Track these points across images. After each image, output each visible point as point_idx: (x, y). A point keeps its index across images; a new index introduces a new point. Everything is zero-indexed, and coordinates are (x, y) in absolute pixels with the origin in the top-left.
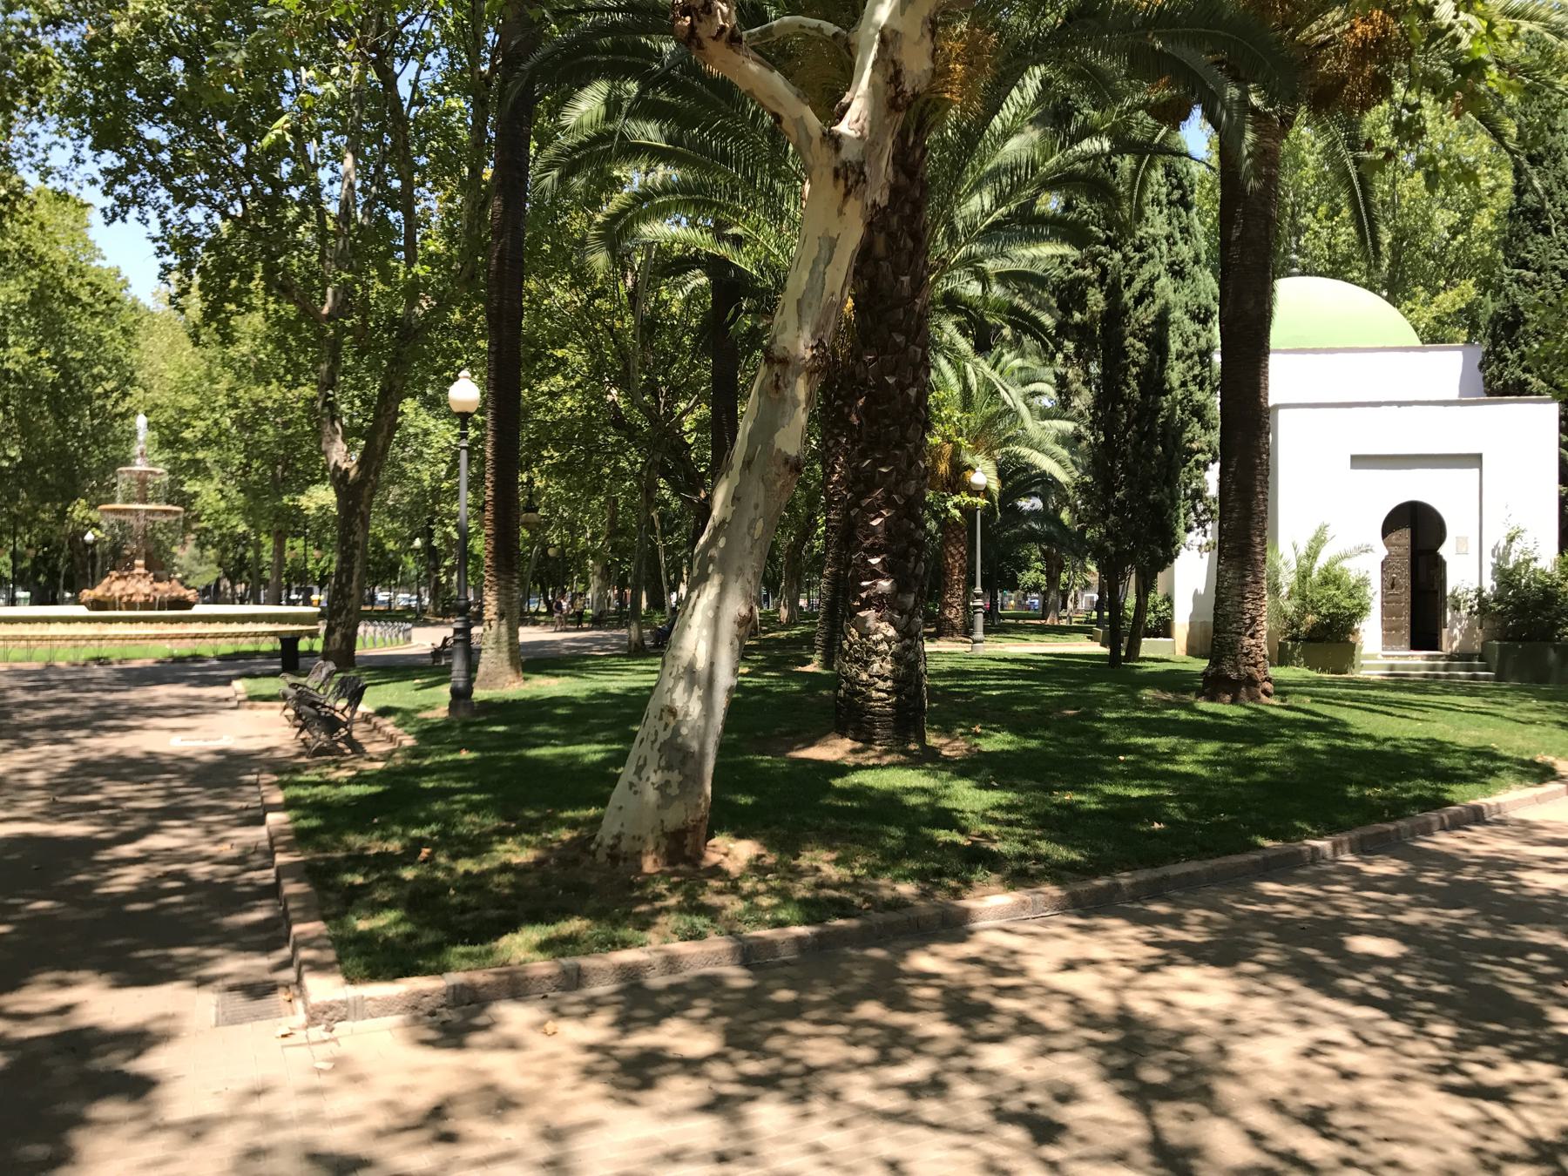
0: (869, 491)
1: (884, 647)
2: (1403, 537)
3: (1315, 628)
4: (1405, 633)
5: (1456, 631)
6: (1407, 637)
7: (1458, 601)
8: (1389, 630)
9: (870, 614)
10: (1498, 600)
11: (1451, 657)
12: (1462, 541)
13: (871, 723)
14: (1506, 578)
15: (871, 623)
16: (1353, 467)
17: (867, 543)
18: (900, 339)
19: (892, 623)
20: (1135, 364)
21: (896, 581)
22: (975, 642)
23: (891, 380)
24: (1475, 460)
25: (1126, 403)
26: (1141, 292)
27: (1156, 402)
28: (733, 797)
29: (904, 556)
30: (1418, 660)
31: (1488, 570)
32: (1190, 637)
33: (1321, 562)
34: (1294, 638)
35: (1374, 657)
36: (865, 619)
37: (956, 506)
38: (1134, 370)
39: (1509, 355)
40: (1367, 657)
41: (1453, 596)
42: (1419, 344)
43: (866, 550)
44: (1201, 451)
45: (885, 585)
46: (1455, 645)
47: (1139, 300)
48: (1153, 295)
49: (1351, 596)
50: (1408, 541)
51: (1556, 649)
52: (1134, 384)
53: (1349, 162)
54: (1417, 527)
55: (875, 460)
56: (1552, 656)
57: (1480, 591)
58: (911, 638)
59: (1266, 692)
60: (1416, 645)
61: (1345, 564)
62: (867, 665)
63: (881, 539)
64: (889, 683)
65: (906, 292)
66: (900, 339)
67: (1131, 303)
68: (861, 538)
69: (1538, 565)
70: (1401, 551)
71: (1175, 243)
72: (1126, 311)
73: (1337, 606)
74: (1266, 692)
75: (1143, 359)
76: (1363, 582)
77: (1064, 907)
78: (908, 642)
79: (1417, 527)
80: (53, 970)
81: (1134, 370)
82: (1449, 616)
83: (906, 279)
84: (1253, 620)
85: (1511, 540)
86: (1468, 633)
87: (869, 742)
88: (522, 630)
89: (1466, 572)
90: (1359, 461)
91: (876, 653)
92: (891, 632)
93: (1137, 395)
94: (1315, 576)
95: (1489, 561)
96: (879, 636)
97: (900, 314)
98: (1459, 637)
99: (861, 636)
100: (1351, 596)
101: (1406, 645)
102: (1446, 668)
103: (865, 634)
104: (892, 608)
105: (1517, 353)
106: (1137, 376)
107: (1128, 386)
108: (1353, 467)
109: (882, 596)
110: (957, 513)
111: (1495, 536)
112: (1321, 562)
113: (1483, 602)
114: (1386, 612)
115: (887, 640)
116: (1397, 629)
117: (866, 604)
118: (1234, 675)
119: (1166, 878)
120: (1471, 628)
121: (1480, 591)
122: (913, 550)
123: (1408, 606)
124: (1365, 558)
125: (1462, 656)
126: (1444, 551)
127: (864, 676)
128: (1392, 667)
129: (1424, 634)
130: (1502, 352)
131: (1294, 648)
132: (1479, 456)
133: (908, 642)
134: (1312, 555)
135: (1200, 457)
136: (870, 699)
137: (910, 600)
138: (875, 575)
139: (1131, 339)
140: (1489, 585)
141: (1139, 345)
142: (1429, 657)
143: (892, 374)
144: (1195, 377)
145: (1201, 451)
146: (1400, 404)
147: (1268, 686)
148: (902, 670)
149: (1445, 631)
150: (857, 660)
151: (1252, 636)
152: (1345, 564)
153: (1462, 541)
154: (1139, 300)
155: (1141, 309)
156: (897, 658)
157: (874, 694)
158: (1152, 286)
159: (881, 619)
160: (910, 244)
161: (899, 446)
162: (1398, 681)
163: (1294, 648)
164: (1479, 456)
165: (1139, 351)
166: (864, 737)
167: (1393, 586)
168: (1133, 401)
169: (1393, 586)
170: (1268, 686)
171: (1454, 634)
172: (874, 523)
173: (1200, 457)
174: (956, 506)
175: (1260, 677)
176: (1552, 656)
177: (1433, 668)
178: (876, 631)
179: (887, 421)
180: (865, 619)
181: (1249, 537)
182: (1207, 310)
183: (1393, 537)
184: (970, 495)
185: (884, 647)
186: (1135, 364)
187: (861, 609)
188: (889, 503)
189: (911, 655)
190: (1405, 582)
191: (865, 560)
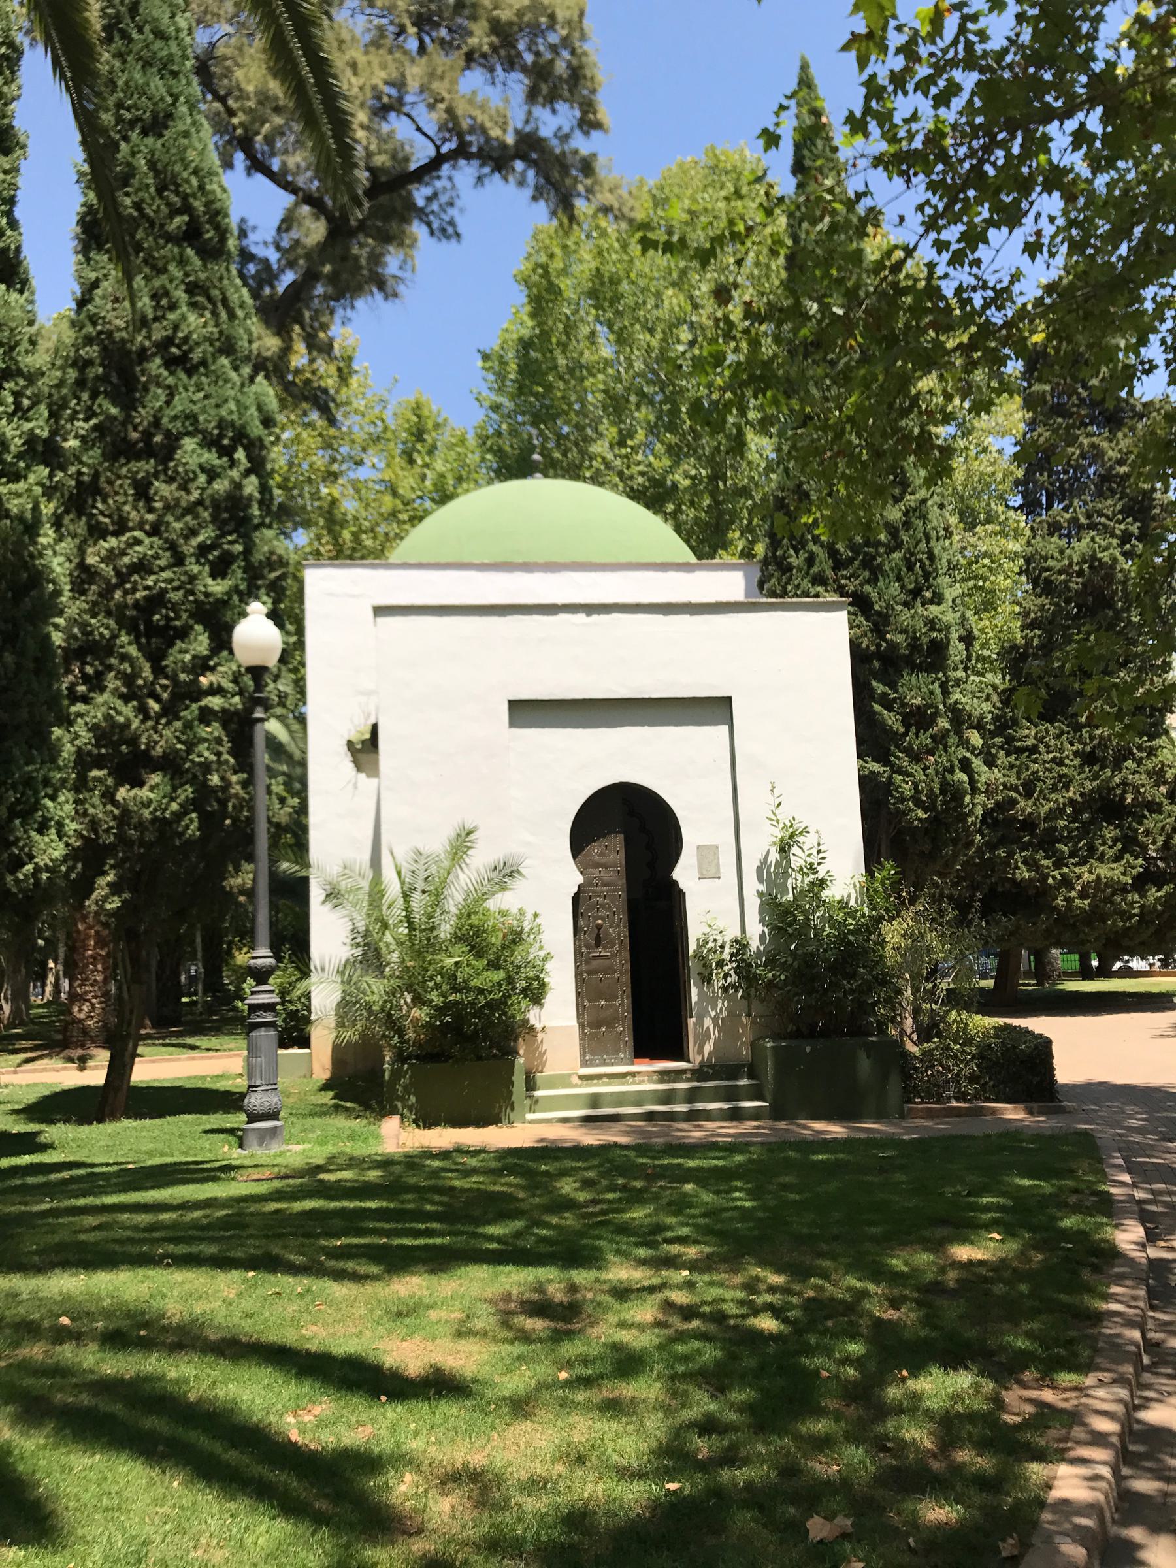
2: (611, 850)
4: (624, 1030)
5: (708, 1023)
6: (628, 1038)
7: (706, 965)
10: (771, 963)
11: (699, 1074)
12: (708, 853)
14: (782, 917)
16: (513, 723)
24: (716, 709)
31: (753, 905)
32: (340, 1054)
33: (454, 901)
35: (562, 1081)
39: (794, 561)
41: (698, 955)
42: (693, 559)
46: (708, 1047)
51: (869, 1048)
54: (629, 830)
56: (864, 1065)
57: (741, 945)
60: (644, 1048)
69: (833, 893)
70: (607, 876)
71: (173, 307)
73: (464, 988)
79: (629, 830)
80: (9, 1214)
82: (694, 991)
86: (727, 1026)
89: (718, 909)
90: (525, 712)
94: (445, 930)
95: (753, 886)
98: (714, 1035)
101: (626, 1052)
102: (692, 1096)
105: (803, 555)
108: (513, 723)
111: (760, 844)
112: (454, 901)
113: (745, 970)
116: (610, 1023)
120: (732, 1015)
121: (741, 945)
123: (627, 978)
124: (545, 897)
126: (678, 874)
129: (655, 1025)
130: (784, 557)
132: (728, 701)
140: (755, 930)
142: (664, 1075)
144: (203, 550)
149: (691, 1021)
164: (728, 701)
167: (598, 942)
169: (598, 942)
171: (708, 1020)
176: (864, 1065)
177: (667, 1097)
190: (618, 931)
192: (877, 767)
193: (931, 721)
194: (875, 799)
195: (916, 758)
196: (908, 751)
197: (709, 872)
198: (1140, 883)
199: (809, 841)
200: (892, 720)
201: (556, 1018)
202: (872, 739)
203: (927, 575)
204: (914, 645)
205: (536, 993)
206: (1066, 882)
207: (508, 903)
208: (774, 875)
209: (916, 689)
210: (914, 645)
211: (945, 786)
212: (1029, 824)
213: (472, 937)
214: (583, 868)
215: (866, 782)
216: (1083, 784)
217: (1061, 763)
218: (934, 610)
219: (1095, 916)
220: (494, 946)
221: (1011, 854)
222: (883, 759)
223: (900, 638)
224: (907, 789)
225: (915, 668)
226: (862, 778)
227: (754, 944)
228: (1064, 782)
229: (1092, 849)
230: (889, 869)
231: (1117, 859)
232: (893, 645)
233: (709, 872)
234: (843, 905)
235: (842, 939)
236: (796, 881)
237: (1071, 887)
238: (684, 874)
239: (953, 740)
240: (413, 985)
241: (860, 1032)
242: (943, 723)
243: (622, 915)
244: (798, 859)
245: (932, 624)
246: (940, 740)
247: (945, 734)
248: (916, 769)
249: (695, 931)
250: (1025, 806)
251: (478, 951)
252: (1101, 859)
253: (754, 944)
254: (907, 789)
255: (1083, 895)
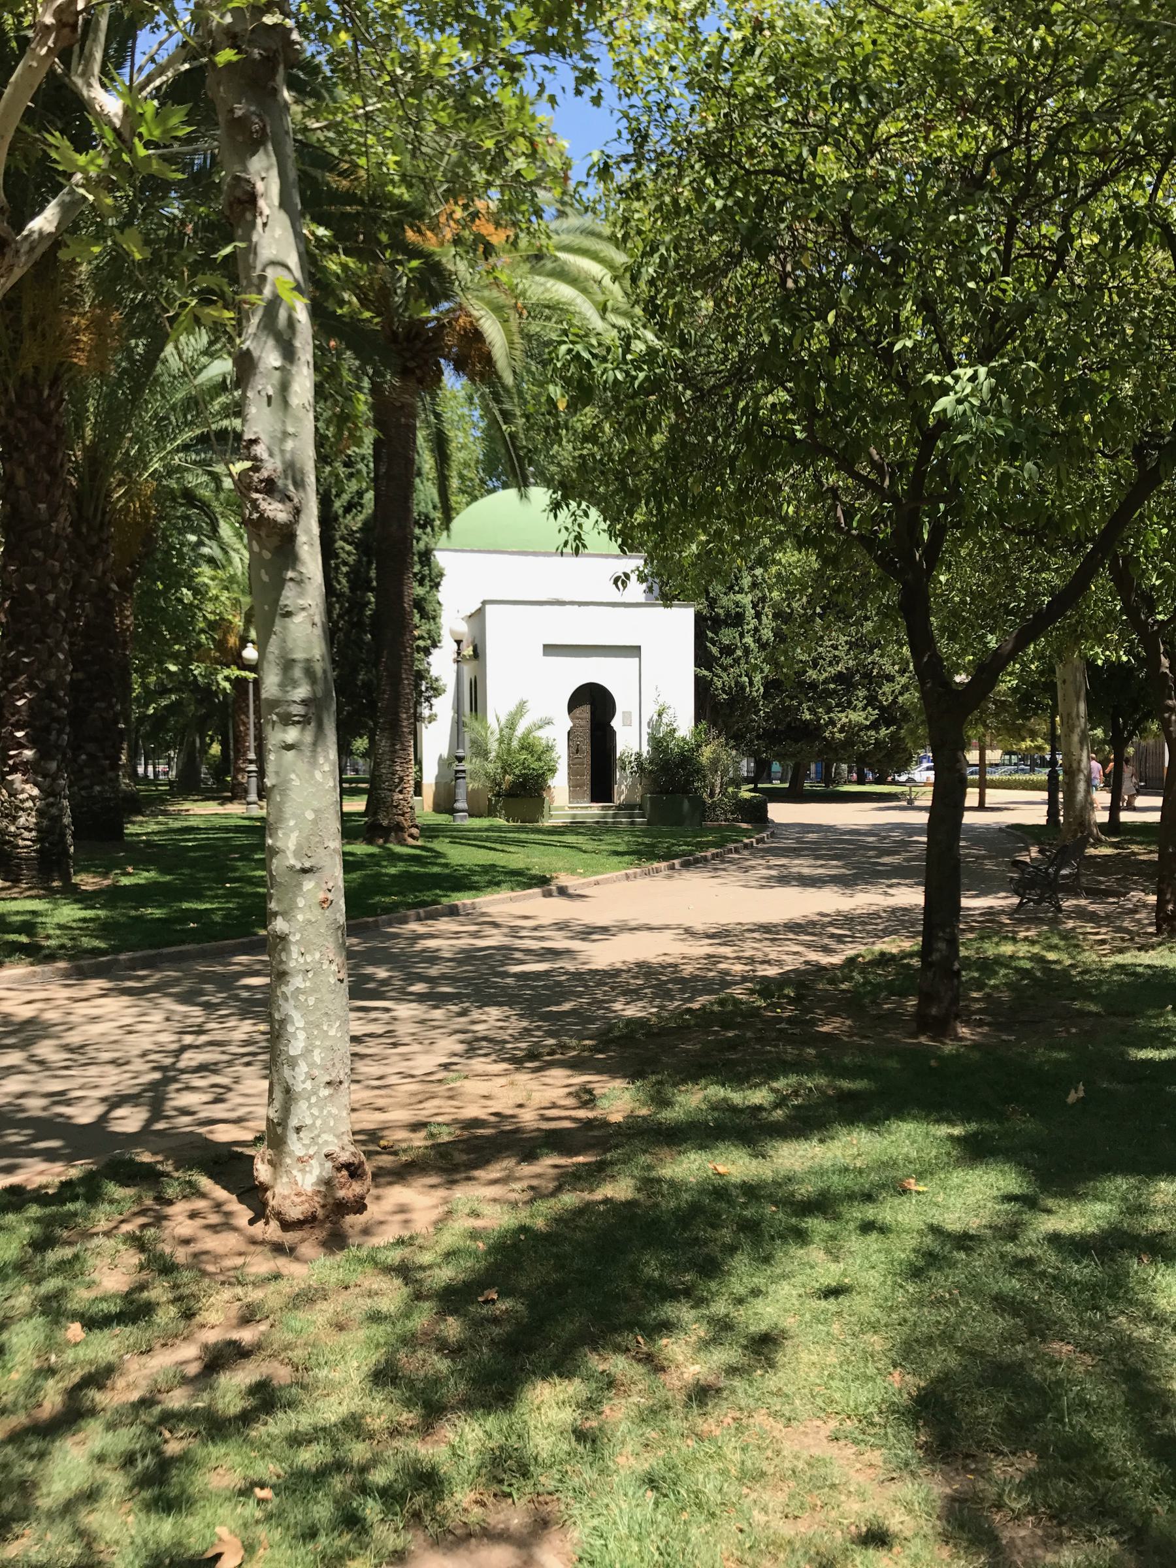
0: (13, 678)
1: (29, 804)
2: (585, 711)
3: (514, 785)
4: (587, 789)
8: (574, 786)
9: (17, 777)
11: (619, 808)
12: (627, 715)
13: (18, 866)
14: (657, 744)
15: (18, 785)
17: (13, 720)
18: (39, 554)
19: (36, 784)
20: (345, 564)
21: (38, 751)
22: (249, 803)
23: (31, 587)
24: (634, 651)
25: (338, 596)
26: (349, 502)
27: (363, 597)
28: (973, 1127)
29: (47, 730)
30: (593, 811)
31: (645, 738)
32: (437, 795)
33: (520, 731)
34: (498, 795)
35: (562, 808)
36: (12, 782)
37: (227, 678)
38: (345, 569)
40: (557, 809)
43: (12, 725)
44: (421, 638)
45: (28, 753)
47: (348, 509)
48: (362, 506)
49: (539, 759)
50: (588, 716)
51: (690, 799)
52: (344, 581)
53: (497, 413)
54: (594, 703)
55: (18, 652)
56: (686, 805)
57: (639, 755)
58: (55, 796)
59: (411, 836)
60: (595, 799)
61: (539, 734)
62: (15, 819)
63: (24, 716)
64: (34, 833)
65: (44, 516)
66: (39, 554)
67: (340, 512)
68: (7, 715)
70: (583, 723)
72: (336, 518)
73: (528, 768)
74: (411, 836)
75: (351, 560)
76: (549, 749)
77: (66, 975)
78: (51, 800)
79: (594, 703)
81: (345, 569)
83: (42, 506)
84: (401, 779)
85: (660, 715)
86: (631, 788)
87: (16, 881)
88: (1043, 821)
89: (630, 740)
91: (23, 810)
92: (35, 792)
93: (346, 590)
94: (515, 744)
95: (646, 730)
96: (25, 796)
97: (39, 533)
99: (10, 795)
100: (539, 759)
101: (588, 798)
103: (13, 794)
104: (36, 773)
106: (347, 574)
107: (339, 583)
109: (27, 762)
110: (227, 685)
111: (650, 712)
112: (520, 731)
114: (573, 772)
115: (32, 798)
117: (14, 770)
118: (385, 823)
119: (160, 955)
120: (633, 785)
121: (639, 755)
122: (55, 725)
124: (557, 731)
125: (627, 807)
126: (613, 724)
127: (12, 829)
128: (574, 816)
129: (601, 789)
131: (497, 802)
132: (638, 649)
133: (51, 800)
134: (512, 725)
135: (421, 643)
136: (18, 847)
137: (53, 766)
138: (20, 746)
139: (340, 543)
140: (646, 749)
141: (348, 548)
143: (32, 582)
145: (421, 638)
146: (580, 604)
147: (415, 831)
148: (45, 822)
150: (7, 816)
151: (401, 792)
152: (539, 734)
153: (627, 715)
154: (348, 509)
155: (349, 517)
156: (41, 813)
157: (21, 843)
158: (361, 497)
159: (26, 782)
160: (47, 478)
161: (40, 641)
162: (575, 827)
163: (497, 802)
164: (638, 649)
165: (349, 553)
166: (12, 877)
168: (342, 594)
170: (415, 831)
171: (624, 787)
172: (19, 703)
173: (421, 643)
174: (227, 678)
175: (406, 824)
176: (686, 805)
177: (605, 816)
178: (23, 791)
179: (28, 620)
180: (12, 782)
181: (397, 714)
182: (427, 516)
183: (577, 712)
184: (240, 669)
185: (29, 804)
186: (345, 564)
187: (10, 773)
188: (31, 687)
189: (54, 811)
190: (586, 747)
191: (12, 733)
192: (706, 673)
193: (734, 651)
194: (702, 688)
195: (725, 669)
196: (721, 666)
197: (627, 723)
198: (875, 726)
199: (670, 712)
200: (715, 650)
201: (559, 785)
202: (702, 658)
203: (737, 579)
204: (728, 614)
205: (553, 770)
206: (832, 722)
207: (544, 735)
208: (655, 726)
209: (727, 636)
210: (728, 614)
211: (737, 683)
212: (813, 685)
213: (526, 746)
214: (572, 719)
215: (698, 680)
216: (847, 662)
217: (836, 648)
218: (739, 597)
219: (848, 743)
220: (541, 753)
221: (800, 704)
222: (709, 669)
223: (721, 611)
224: (719, 684)
225: (728, 625)
226: (696, 676)
227: (645, 755)
228: (836, 660)
229: (850, 702)
230: (704, 725)
231: (864, 709)
232: (718, 614)
233: (627, 723)
234: (684, 739)
235: (682, 754)
236: (663, 729)
237: (834, 725)
238: (616, 723)
239: (743, 661)
240: (506, 768)
241: (687, 792)
242: (739, 653)
243: (588, 741)
244: (665, 719)
245: (737, 604)
246: (737, 661)
247: (739, 658)
248: (724, 675)
249: (620, 749)
250: (812, 674)
251: (532, 753)
252: (854, 709)
253: (645, 755)
254: (719, 684)
255: (841, 731)
